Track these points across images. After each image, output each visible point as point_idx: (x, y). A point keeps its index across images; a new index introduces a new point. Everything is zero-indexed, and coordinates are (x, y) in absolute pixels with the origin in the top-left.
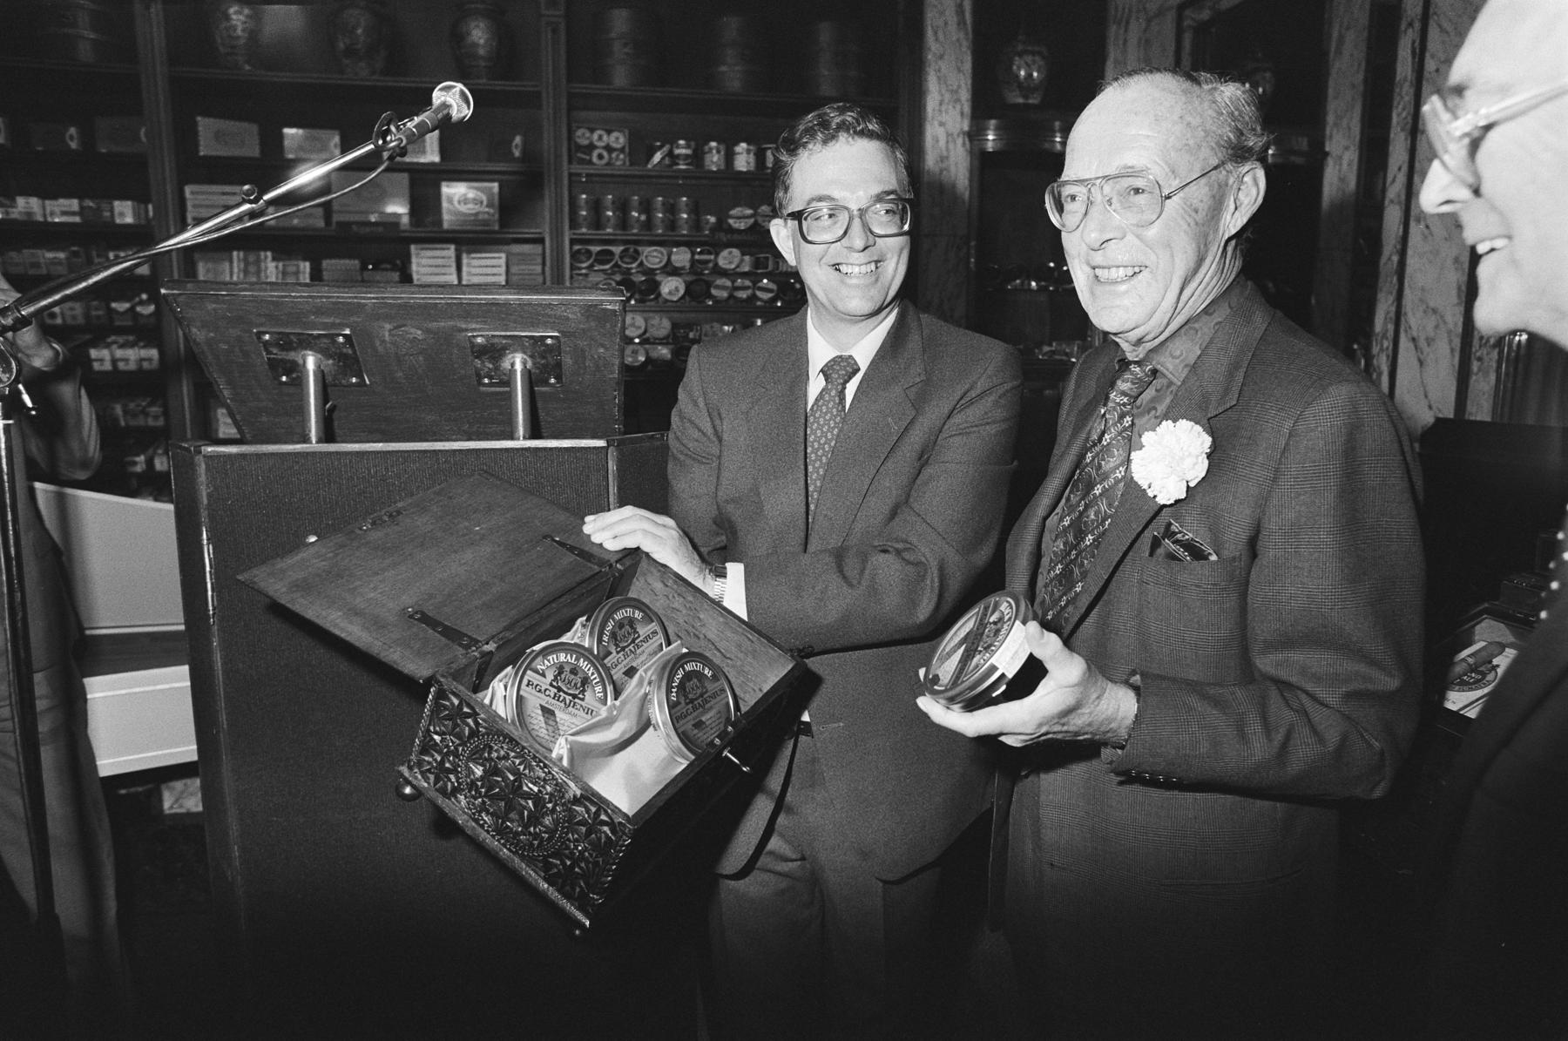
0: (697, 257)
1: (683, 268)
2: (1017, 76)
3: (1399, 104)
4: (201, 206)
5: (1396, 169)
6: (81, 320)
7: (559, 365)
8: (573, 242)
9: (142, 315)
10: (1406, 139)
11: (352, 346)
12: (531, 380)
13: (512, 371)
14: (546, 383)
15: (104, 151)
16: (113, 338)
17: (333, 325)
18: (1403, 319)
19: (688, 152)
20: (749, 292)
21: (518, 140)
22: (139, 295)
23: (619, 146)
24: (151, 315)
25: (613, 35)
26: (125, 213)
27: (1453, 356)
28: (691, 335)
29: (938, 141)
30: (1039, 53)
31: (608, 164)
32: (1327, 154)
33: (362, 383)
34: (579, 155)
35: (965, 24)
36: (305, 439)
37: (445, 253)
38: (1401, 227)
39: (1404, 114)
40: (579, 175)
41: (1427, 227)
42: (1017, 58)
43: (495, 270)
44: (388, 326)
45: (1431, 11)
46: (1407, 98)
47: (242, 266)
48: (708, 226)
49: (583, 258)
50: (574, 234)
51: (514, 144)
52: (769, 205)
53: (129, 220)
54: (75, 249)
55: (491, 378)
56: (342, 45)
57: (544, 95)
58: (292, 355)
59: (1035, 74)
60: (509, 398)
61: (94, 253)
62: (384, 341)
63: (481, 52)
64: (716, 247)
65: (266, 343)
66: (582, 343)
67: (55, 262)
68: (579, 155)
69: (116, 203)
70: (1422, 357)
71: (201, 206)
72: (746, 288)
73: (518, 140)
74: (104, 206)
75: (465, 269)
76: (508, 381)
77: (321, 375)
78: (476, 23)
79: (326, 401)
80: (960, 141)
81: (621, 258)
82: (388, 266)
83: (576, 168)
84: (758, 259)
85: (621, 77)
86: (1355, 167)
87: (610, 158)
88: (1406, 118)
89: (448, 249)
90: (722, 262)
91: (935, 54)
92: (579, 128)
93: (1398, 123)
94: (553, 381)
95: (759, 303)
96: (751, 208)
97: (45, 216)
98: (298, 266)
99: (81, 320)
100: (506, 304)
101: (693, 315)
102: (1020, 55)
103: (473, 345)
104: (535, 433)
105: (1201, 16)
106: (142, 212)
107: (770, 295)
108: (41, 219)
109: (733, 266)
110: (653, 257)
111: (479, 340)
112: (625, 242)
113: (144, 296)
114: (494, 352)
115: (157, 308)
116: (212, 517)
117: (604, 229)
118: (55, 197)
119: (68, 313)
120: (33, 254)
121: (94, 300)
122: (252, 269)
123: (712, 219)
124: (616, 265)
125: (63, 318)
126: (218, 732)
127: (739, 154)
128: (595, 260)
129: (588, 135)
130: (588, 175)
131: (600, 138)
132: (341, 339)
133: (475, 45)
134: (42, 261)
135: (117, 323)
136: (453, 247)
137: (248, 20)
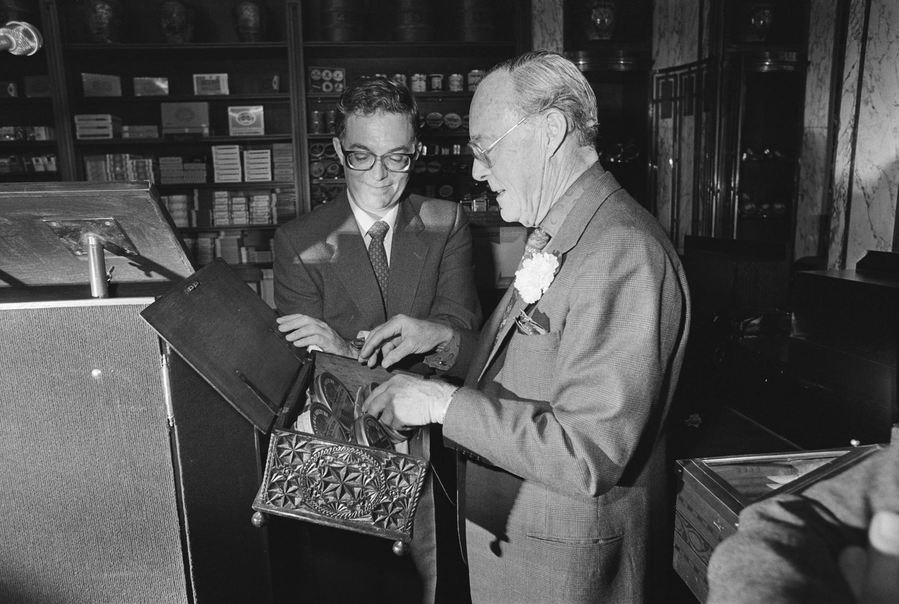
2: (595, 22)
3: (853, 19)
5: (855, 67)
8: (309, 140)
10: (858, 45)
15: (30, 97)
18: (855, 174)
21: (276, 78)
25: (332, 9)
26: (42, 134)
27: (892, 199)
32: (809, 63)
34: (314, 86)
37: (233, 151)
38: (854, 108)
39: (857, 27)
40: (317, 99)
41: (873, 107)
42: (594, 11)
43: (264, 161)
46: (859, 15)
49: (317, 151)
50: (310, 136)
51: (273, 81)
52: (461, 115)
54: (13, 157)
56: (165, 26)
57: (289, 50)
59: (606, 20)
61: (24, 159)
63: (251, 24)
68: (314, 86)
70: (869, 201)
73: (276, 78)
75: (245, 160)
78: (245, 7)
82: (199, 160)
85: (338, 36)
86: (830, 70)
87: (334, 88)
88: (858, 29)
89: (235, 148)
91: (538, 11)
92: (313, 69)
93: (852, 34)
98: (144, 162)
102: (596, 8)
117: (329, 132)
127: (415, 81)
128: (325, 152)
129: (319, 73)
130: (322, 99)
131: (327, 74)
133: (247, 20)
136: (237, 147)
137: (109, 13)
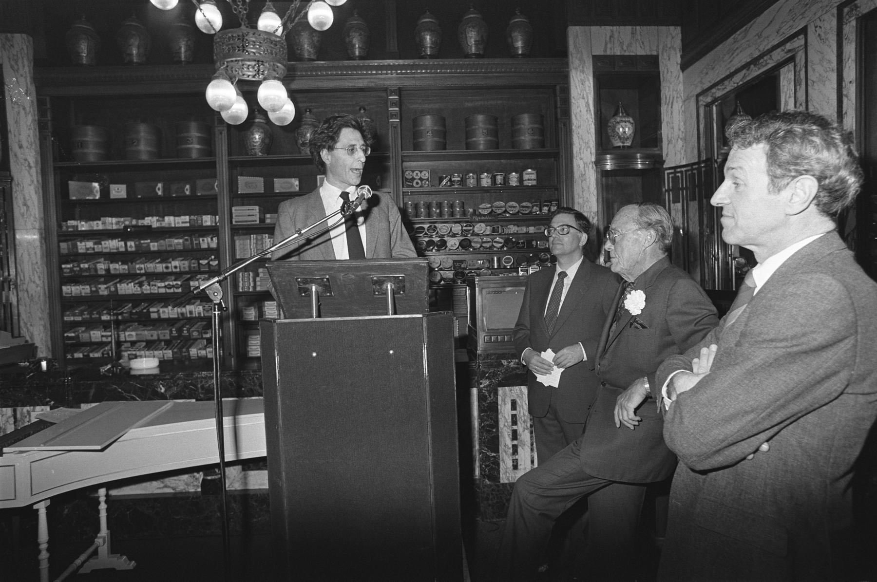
0: (464, 228)
1: (457, 234)
4: (239, 216)
6: (187, 269)
7: (404, 286)
9: (212, 266)
11: (329, 282)
12: (394, 293)
13: (387, 289)
14: (399, 293)
16: (199, 276)
17: (323, 275)
19: (459, 179)
20: (490, 244)
22: (211, 257)
23: (426, 178)
24: (216, 265)
26: (207, 220)
28: (462, 266)
29: (579, 167)
30: (629, 122)
31: (421, 187)
33: (331, 296)
35: (590, 111)
36: (312, 317)
44: (343, 274)
45: (809, 99)
47: (255, 242)
48: (469, 213)
53: (209, 224)
54: (186, 238)
55: (378, 292)
58: (307, 286)
60: (386, 299)
62: (340, 280)
64: (471, 223)
65: (299, 282)
66: (413, 278)
67: (178, 244)
69: (204, 217)
71: (239, 216)
72: (489, 242)
74: (199, 218)
76: (386, 293)
77: (317, 292)
79: (319, 302)
80: (591, 166)
81: (428, 230)
83: (405, 189)
84: (494, 228)
90: (476, 230)
94: (402, 292)
95: (495, 249)
96: (489, 204)
97: (175, 224)
99: (187, 269)
100: (385, 265)
101: (463, 256)
103: (372, 280)
104: (395, 313)
105: (707, 100)
106: (214, 220)
107: (501, 245)
108: (173, 226)
109: (482, 232)
110: (443, 228)
111: (375, 278)
112: (430, 223)
113: (213, 257)
114: (380, 282)
115: (219, 262)
116: (279, 345)
118: (179, 216)
119: (182, 266)
120: (169, 241)
121: (193, 259)
122: (260, 242)
123: (471, 210)
124: (426, 234)
125: (180, 268)
126: (278, 428)
129: (411, 174)
131: (417, 174)
132: (325, 280)
134: (173, 244)
135: (202, 270)
